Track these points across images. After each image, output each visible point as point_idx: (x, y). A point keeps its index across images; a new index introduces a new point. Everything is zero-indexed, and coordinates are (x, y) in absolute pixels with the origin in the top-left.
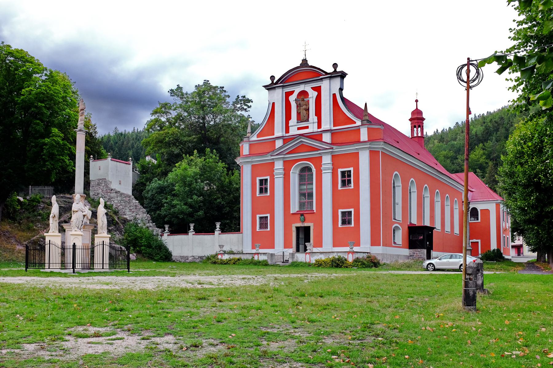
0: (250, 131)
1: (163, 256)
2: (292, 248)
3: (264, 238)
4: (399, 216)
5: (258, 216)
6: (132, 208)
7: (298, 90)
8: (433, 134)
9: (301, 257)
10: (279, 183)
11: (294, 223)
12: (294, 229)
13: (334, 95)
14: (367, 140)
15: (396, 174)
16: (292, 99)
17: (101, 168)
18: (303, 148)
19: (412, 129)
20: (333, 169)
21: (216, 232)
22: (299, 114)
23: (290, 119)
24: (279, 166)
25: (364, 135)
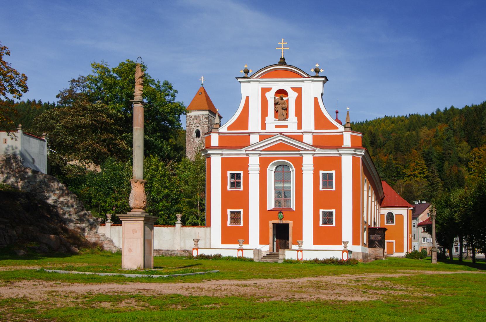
2: (268, 244)
3: (235, 233)
5: (229, 211)
8: (181, 119)
12: (271, 226)
13: (316, 99)
14: (350, 146)
16: (271, 97)
18: (281, 147)
21: (177, 225)
23: (267, 115)
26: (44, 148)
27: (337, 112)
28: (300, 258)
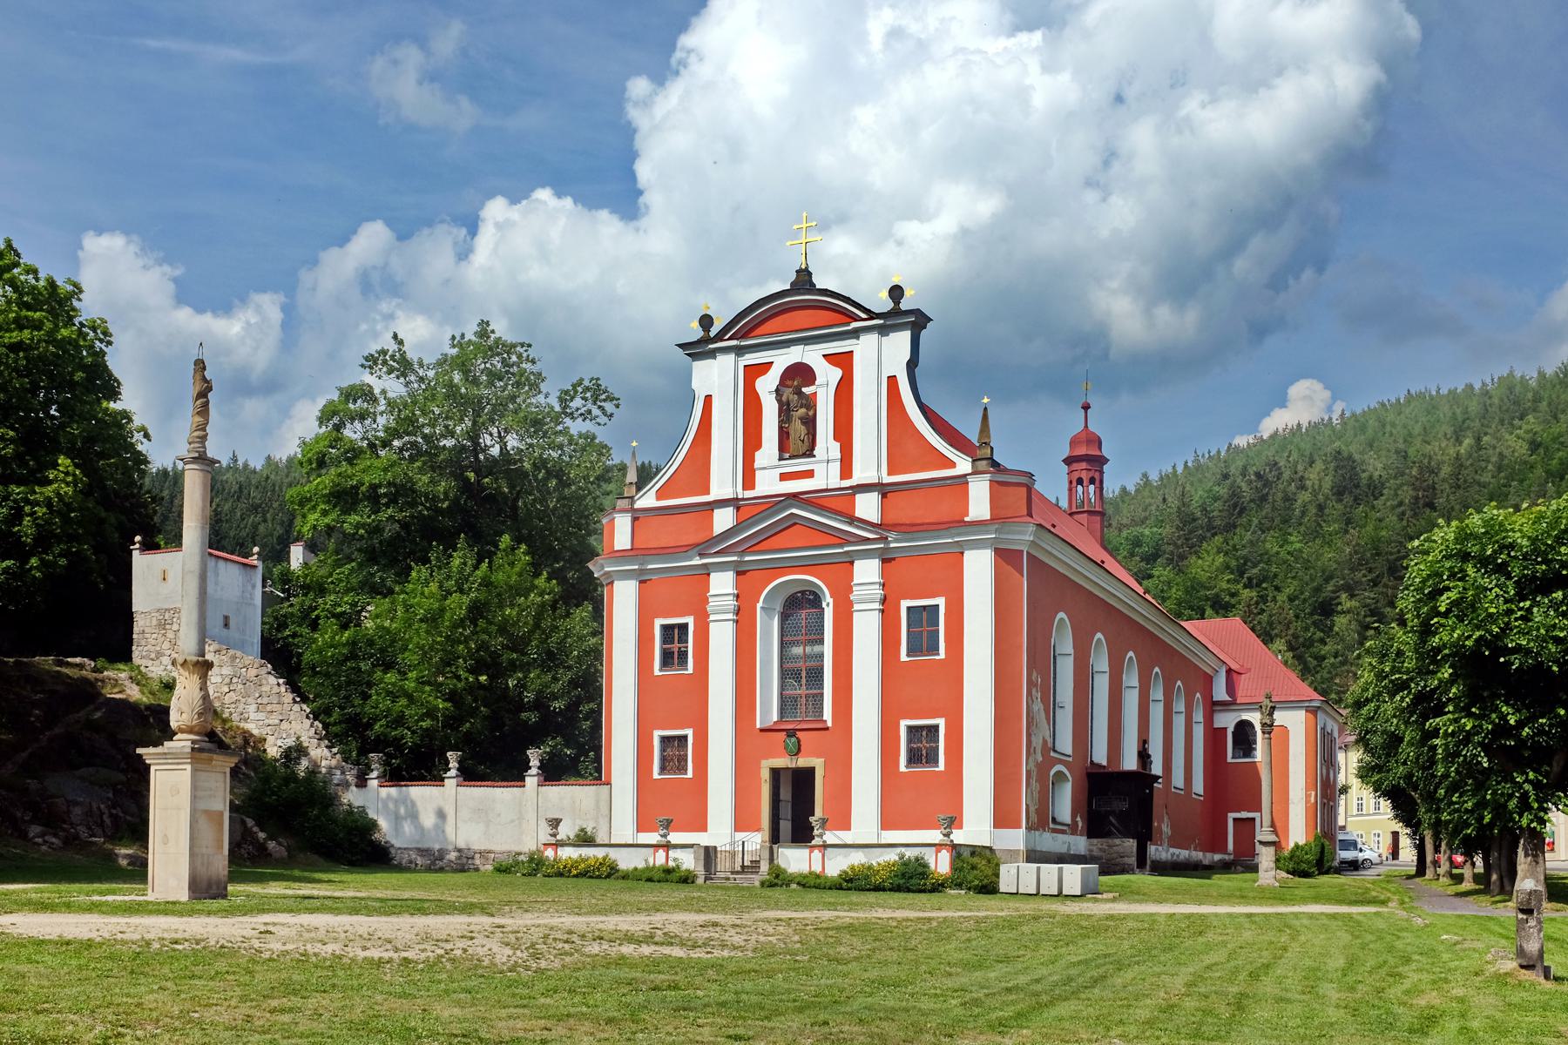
0: (634, 479)
1: (359, 849)
3: (672, 794)
4: (1066, 744)
6: (265, 700)
7: (782, 360)
9: (795, 859)
10: (722, 637)
11: (766, 758)
12: (765, 775)
13: (892, 380)
15: (1062, 619)
16: (767, 385)
17: (170, 577)
19: (1070, 490)
20: (884, 601)
21: (528, 779)
22: (784, 435)
23: (759, 446)
24: (722, 584)
25: (979, 503)
26: (254, 586)
27: (1086, 407)
28: (817, 868)
